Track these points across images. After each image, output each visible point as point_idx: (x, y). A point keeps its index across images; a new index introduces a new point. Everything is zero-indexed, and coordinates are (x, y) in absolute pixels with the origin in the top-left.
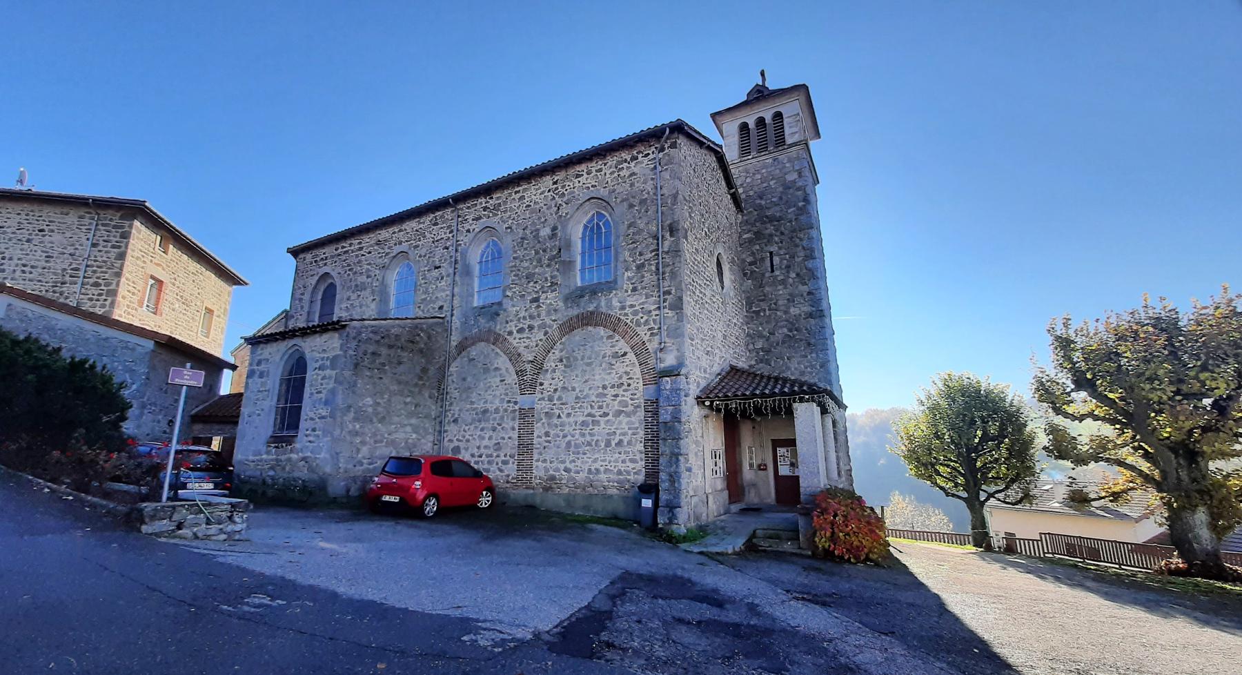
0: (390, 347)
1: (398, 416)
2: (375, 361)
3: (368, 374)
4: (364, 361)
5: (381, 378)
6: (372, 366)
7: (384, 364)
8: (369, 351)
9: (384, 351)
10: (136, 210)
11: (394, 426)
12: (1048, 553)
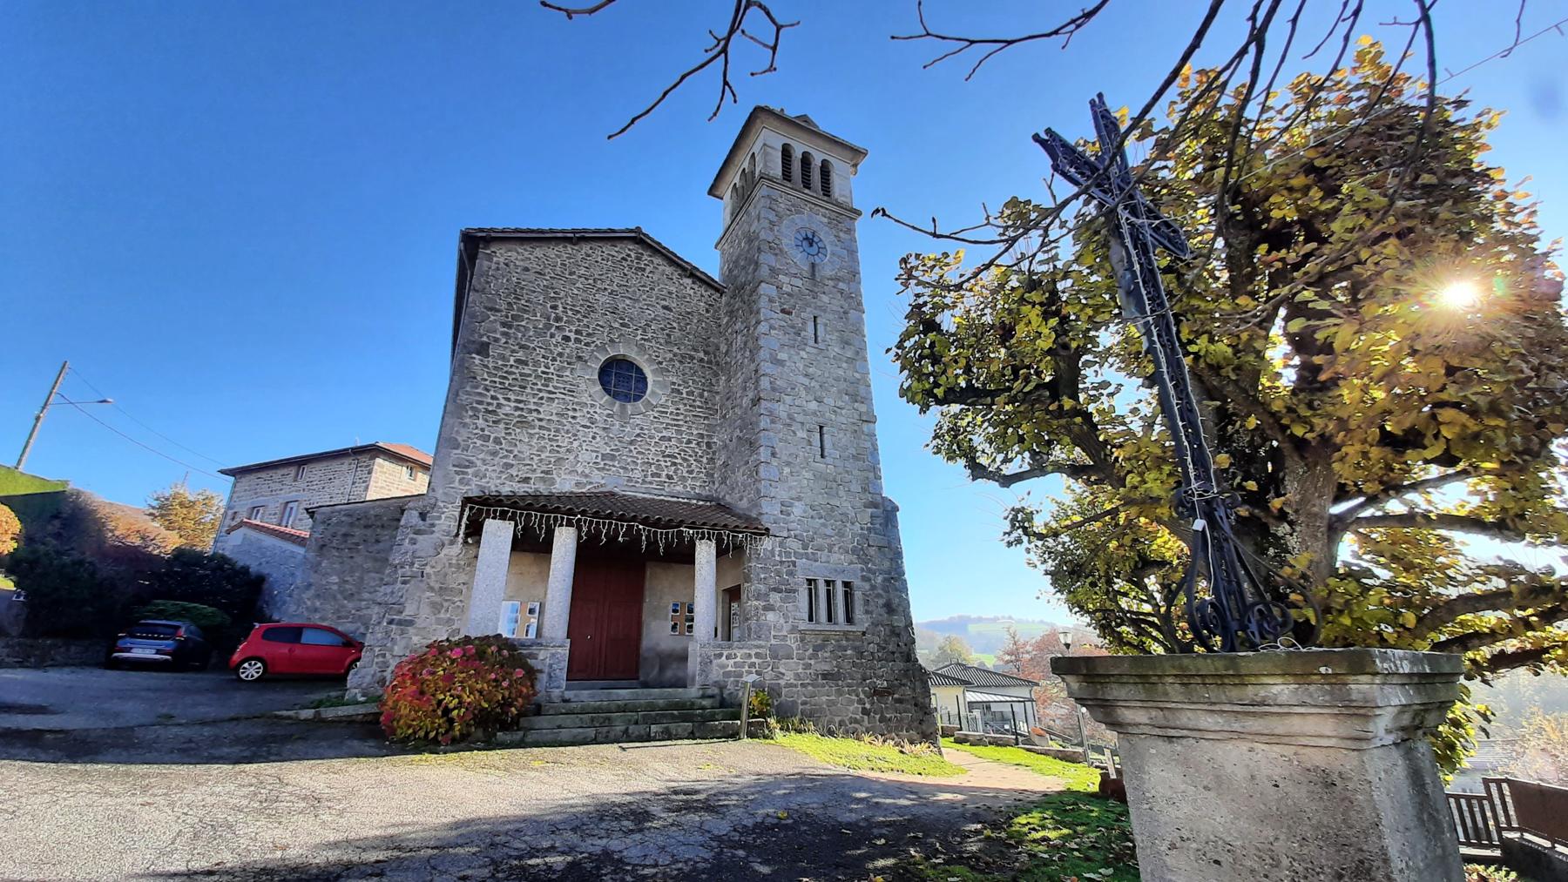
0: (366, 527)
1: (370, 593)
2: (346, 542)
3: (337, 554)
4: (332, 542)
5: (352, 557)
6: (343, 546)
7: (357, 544)
8: (340, 533)
9: (358, 532)
10: (373, 451)
11: (364, 603)
12: (1511, 829)
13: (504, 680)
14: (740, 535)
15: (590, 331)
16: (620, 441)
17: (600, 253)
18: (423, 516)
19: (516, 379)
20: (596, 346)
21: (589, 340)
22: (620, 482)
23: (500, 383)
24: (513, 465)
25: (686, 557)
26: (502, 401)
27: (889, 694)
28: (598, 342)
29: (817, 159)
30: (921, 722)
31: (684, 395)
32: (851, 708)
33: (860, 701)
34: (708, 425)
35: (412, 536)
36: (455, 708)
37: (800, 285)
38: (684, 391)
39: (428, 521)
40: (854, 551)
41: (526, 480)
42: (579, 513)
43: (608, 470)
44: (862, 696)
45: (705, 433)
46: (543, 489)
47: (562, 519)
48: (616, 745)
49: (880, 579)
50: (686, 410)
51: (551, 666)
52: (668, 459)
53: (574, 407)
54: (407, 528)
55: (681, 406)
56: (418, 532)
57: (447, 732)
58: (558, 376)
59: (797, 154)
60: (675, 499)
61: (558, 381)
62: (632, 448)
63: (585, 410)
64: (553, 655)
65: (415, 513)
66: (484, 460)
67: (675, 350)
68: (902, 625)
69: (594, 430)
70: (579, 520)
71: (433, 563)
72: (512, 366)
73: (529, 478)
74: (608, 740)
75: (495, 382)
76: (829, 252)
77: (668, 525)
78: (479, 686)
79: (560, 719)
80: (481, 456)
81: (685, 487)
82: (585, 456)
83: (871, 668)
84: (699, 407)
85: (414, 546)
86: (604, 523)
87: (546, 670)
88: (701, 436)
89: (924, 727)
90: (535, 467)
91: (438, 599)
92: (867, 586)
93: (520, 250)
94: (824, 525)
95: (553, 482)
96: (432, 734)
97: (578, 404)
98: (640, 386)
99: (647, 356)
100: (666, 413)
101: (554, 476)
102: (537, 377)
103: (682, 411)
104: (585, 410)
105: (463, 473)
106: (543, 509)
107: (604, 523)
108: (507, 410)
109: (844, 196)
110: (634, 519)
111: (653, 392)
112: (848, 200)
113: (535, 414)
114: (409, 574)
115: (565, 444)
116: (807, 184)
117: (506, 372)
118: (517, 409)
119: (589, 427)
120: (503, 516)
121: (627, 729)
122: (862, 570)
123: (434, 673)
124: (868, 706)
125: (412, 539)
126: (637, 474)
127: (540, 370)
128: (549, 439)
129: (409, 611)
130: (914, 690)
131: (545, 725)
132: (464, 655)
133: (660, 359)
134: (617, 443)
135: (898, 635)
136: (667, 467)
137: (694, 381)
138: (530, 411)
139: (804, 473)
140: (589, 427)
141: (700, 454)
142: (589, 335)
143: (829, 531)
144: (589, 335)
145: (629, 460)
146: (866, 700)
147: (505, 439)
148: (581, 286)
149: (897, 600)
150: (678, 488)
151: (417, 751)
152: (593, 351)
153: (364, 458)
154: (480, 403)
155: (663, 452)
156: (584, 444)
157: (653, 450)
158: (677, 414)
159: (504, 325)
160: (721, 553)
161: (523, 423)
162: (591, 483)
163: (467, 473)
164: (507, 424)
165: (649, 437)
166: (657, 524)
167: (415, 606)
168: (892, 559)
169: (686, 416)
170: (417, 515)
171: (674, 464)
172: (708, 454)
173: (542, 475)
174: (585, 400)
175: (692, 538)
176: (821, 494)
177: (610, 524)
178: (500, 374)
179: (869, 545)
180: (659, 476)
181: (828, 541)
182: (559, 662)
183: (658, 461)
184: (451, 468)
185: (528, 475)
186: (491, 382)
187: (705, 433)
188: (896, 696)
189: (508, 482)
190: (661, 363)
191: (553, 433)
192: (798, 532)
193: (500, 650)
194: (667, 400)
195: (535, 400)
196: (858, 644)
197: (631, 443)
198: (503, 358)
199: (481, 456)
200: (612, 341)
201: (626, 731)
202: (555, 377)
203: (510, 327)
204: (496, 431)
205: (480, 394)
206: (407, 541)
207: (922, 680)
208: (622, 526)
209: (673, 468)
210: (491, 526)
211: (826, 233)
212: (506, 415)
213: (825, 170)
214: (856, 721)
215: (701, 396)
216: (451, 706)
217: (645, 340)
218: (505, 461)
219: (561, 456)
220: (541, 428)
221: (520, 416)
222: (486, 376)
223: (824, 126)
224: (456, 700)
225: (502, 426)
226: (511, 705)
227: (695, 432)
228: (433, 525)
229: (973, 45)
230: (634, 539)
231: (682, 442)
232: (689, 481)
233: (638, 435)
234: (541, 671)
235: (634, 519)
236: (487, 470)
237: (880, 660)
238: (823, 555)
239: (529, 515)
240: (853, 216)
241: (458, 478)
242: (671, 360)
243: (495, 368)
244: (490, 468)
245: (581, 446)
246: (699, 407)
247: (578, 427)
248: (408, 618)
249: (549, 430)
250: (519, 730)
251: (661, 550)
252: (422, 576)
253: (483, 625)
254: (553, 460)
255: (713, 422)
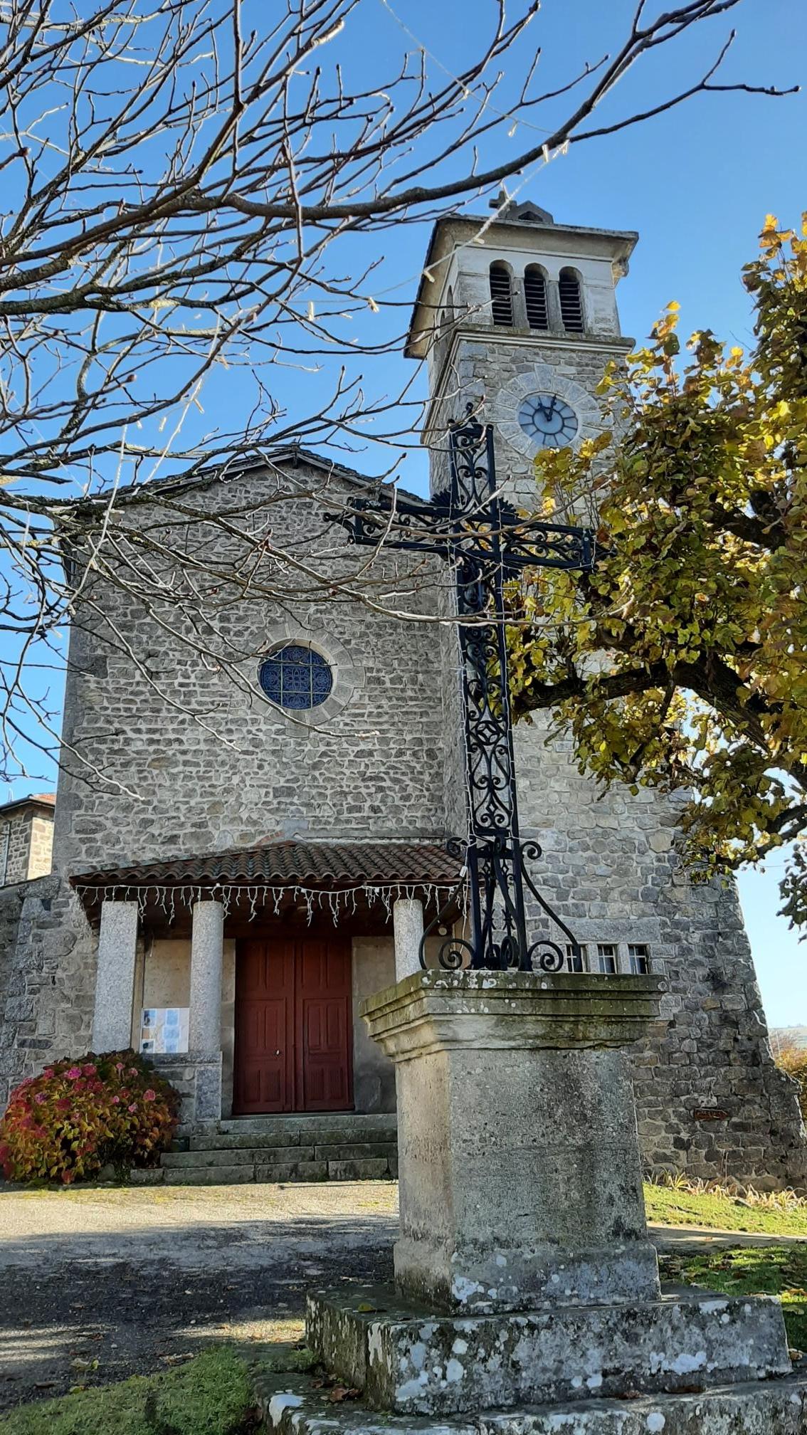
13: (132, 1103)
14: (451, 888)
15: (241, 613)
16: (298, 767)
17: (243, 495)
18: (46, 904)
19: (146, 701)
20: (251, 633)
21: (240, 627)
22: (304, 825)
23: (127, 710)
24: (153, 821)
25: (383, 930)
26: (131, 735)
27: (722, 1117)
28: (253, 628)
29: (552, 271)
30: (784, 1159)
31: (388, 685)
32: (656, 1139)
33: (671, 1128)
34: (428, 724)
35: (35, 931)
36: (75, 1139)
37: (533, 490)
38: (387, 679)
39: (54, 910)
40: (646, 896)
41: (173, 839)
42: (218, 881)
43: (284, 811)
44: (674, 1120)
45: (424, 736)
46: (196, 849)
47: (196, 891)
48: (277, 1184)
49: (696, 937)
50: (391, 707)
51: (200, 1088)
52: (370, 784)
53: (229, 726)
54: (29, 921)
55: (384, 702)
56: (42, 926)
57: (69, 1167)
58: (202, 686)
59: (518, 272)
60: (386, 842)
61: (202, 694)
62: (317, 773)
63: (245, 730)
64: (202, 1073)
65: (36, 901)
66: (114, 820)
67: (369, 618)
68: (741, 1007)
69: (260, 756)
70: (219, 890)
71: (65, 964)
72: (138, 683)
73: (175, 836)
74: (269, 1179)
75: (119, 709)
76: (580, 422)
77: (342, 885)
78: (100, 1112)
79: (209, 1156)
80: (110, 815)
81: (400, 821)
82: (250, 795)
83: (688, 1077)
84: (411, 699)
85: (40, 944)
86: (253, 891)
87: (195, 1094)
88: (419, 742)
89: (789, 1168)
90: (183, 819)
91: (76, 1012)
92: (673, 949)
93: (132, 516)
94: (592, 860)
95: (209, 838)
96: (54, 1170)
97: (232, 721)
98: (322, 680)
99: (326, 636)
100: (362, 715)
101: (210, 829)
102: (174, 692)
103: (386, 708)
104: (245, 730)
105: (91, 840)
106: (170, 881)
107: (253, 891)
108: (139, 746)
109: (604, 320)
110: (294, 880)
111: (340, 688)
112: (612, 325)
113: (176, 746)
114: (38, 980)
115: (221, 782)
116: (538, 320)
117: (132, 693)
118: (151, 742)
119: (253, 753)
120: (120, 896)
121: (296, 1166)
122: (664, 924)
123: (48, 1098)
124: (684, 1135)
125: (35, 935)
126: (327, 812)
127: (176, 682)
128: (198, 777)
129: (43, 1028)
130: (768, 1109)
131: (192, 1162)
132: (83, 1075)
133: (346, 637)
134: (293, 769)
135: (735, 1024)
136: (370, 795)
137: (400, 660)
138: (169, 742)
139: (552, 783)
140: (253, 753)
141: (418, 767)
142: (239, 619)
143: (602, 869)
144: (239, 619)
145: (314, 792)
146: (681, 1126)
147: (139, 786)
148: (222, 550)
149: (729, 969)
150: (389, 824)
151: (35, 1187)
152: (247, 641)
153: (18, 819)
154: (102, 740)
155: (363, 774)
156: (247, 778)
157: (347, 772)
158: (379, 715)
159: (123, 627)
160: (428, 917)
161: (162, 761)
162: (262, 832)
163: (94, 840)
164: (139, 765)
165: (341, 755)
166: (326, 884)
167: (49, 1023)
168: (716, 904)
169: (392, 716)
170: (39, 903)
171: (381, 789)
172: (431, 767)
173: (193, 830)
174: (241, 714)
175: (379, 899)
176: (583, 812)
177: (261, 891)
178: (124, 696)
179: (674, 885)
180: (359, 809)
181: (601, 884)
182: (211, 1082)
183: (356, 787)
184: (73, 835)
185: (175, 832)
186: (113, 709)
187: (424, 736)
188: (735, 1119)
189: (148, 846)
190: (348, 642)
191: (202, 769)
192: (549, 874)
193: (128, 1067)
194: (361, 697)
195: (175, 726)
196: (662, 1040)
197: (315, 766)
198: (125, 673)
199: (110, 815)
200: (273, 622)
201: (294, 1169)
202: (197, 689)
203: (130, 629)
204: (127, 778)
205: (101, 729)
206: (31, 938)
207: (782, 1094)
208: (278, 892)
209: (380, 795)
210: (109, 909)
211: (575, 390)
212: (138, 753)
213: (569, 281)
214: (665, 1158)
215: (414, 681)
216: (70, 1136)
217: (321, 612)
218: (142, 817)
219: (217, 799)
220: (186, 763)
221: (156, 752)
222: (106, 704)
223: (563, 217)
224: (77, 1130)
225: (133, 769)
226: (145, 1135)
227: (409, 737)
228: (60, 915)
229: (699, 83)
230: (291, 907)
231: (388, 756)
232: (406, 812)
233: (324, 754)
234: (188, 1095)
235: (294, 880)
236: (119, 832)
237: (703, 1063)
238: (593, 907)
239: (152, 892)
240: (620, 349)
241: (84, 848)
242: (363, 635)
243: (117, 690)
244: (124, 830)
245: (243, 781)
246: (411, 699)
247: (237, 755)
248: (41, 1038)
249: (197, 765)
250: (159, 1167)
251: (335, 920)
252: (54, 982)
253: (110, 1039)
254: (206, 807)
255: (436, 718)
